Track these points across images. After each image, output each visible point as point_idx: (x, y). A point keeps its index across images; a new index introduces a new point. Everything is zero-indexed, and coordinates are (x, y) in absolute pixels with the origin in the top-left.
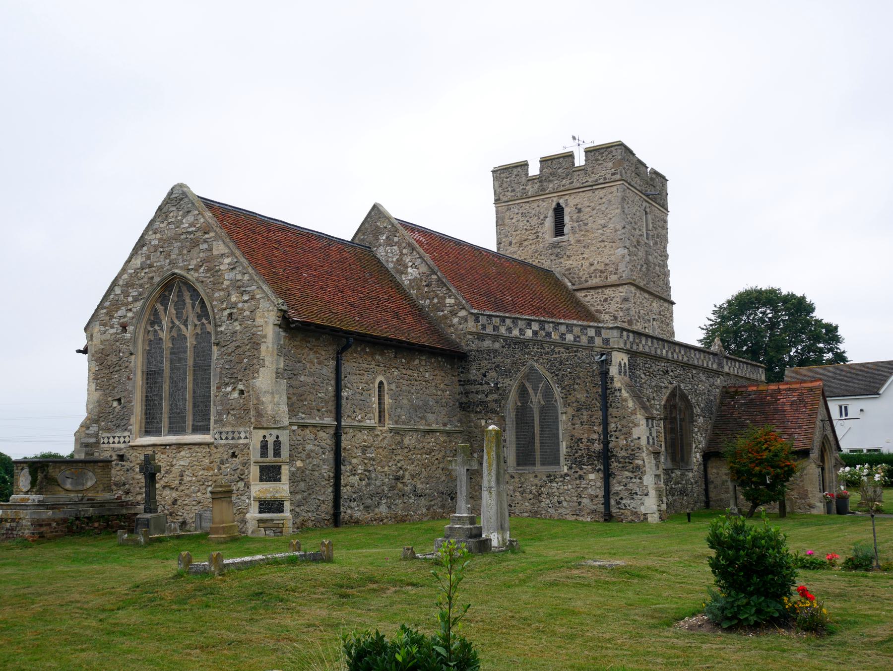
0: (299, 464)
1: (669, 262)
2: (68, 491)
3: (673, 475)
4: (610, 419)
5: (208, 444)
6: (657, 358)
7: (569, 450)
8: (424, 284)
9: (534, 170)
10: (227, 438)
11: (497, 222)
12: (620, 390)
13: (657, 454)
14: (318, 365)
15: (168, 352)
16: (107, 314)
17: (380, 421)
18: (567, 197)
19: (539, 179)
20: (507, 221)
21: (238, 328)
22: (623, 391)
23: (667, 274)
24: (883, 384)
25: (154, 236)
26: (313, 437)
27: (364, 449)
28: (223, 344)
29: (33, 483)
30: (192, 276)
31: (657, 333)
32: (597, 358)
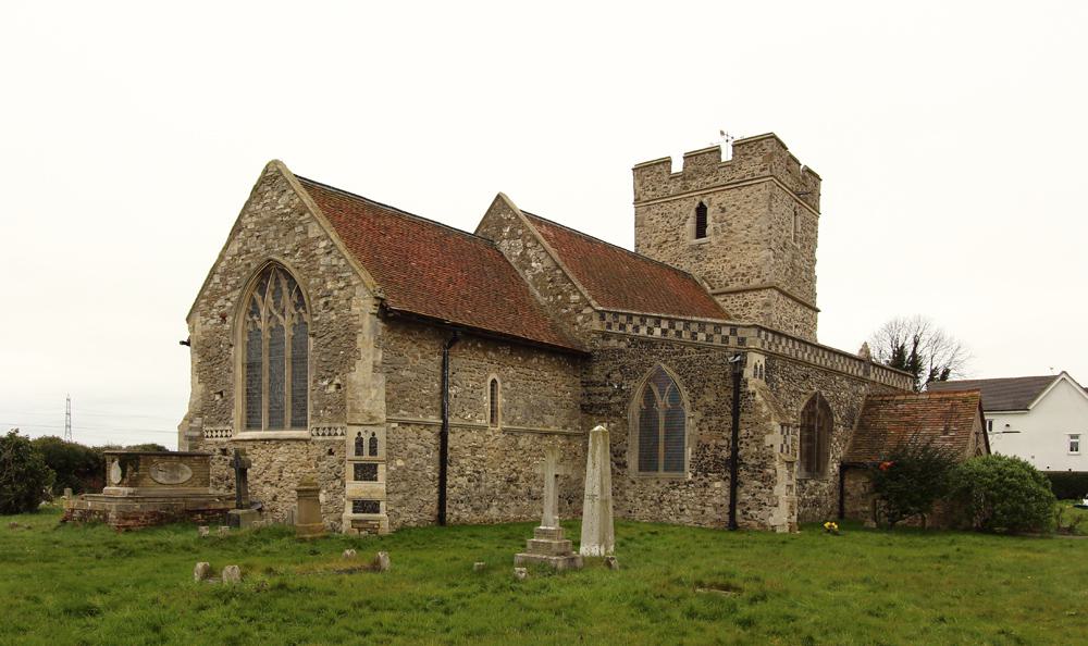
0: (400, 463)
1: (817, 268)
2: (160, 481)
3: (807, 485)
4: (741, 424)
5: (306, 441)
6: (796, 362)
7: (695, 456)
8: (549, 279)
9: (677, 167)
10: (323, 435)
11: (636, 223)
12: (754, 394)
13: (790, 464)
14: (422, 359)
15: (267, 343)
16: (207, 304)
17: (492, 421)
18: (710, 196)
19: (683, 176)
20: (647, 222)
21: (334, 317)
22: (758, 396)
23: (813, 280)
24: (1033, 400)
25: (249, 220)
26: (415, 435)
27: (474, 450)
28: (318, 335)
29: (123, 476)
30: (288, 263)
31: (797, 333)
32: (730, 359)
